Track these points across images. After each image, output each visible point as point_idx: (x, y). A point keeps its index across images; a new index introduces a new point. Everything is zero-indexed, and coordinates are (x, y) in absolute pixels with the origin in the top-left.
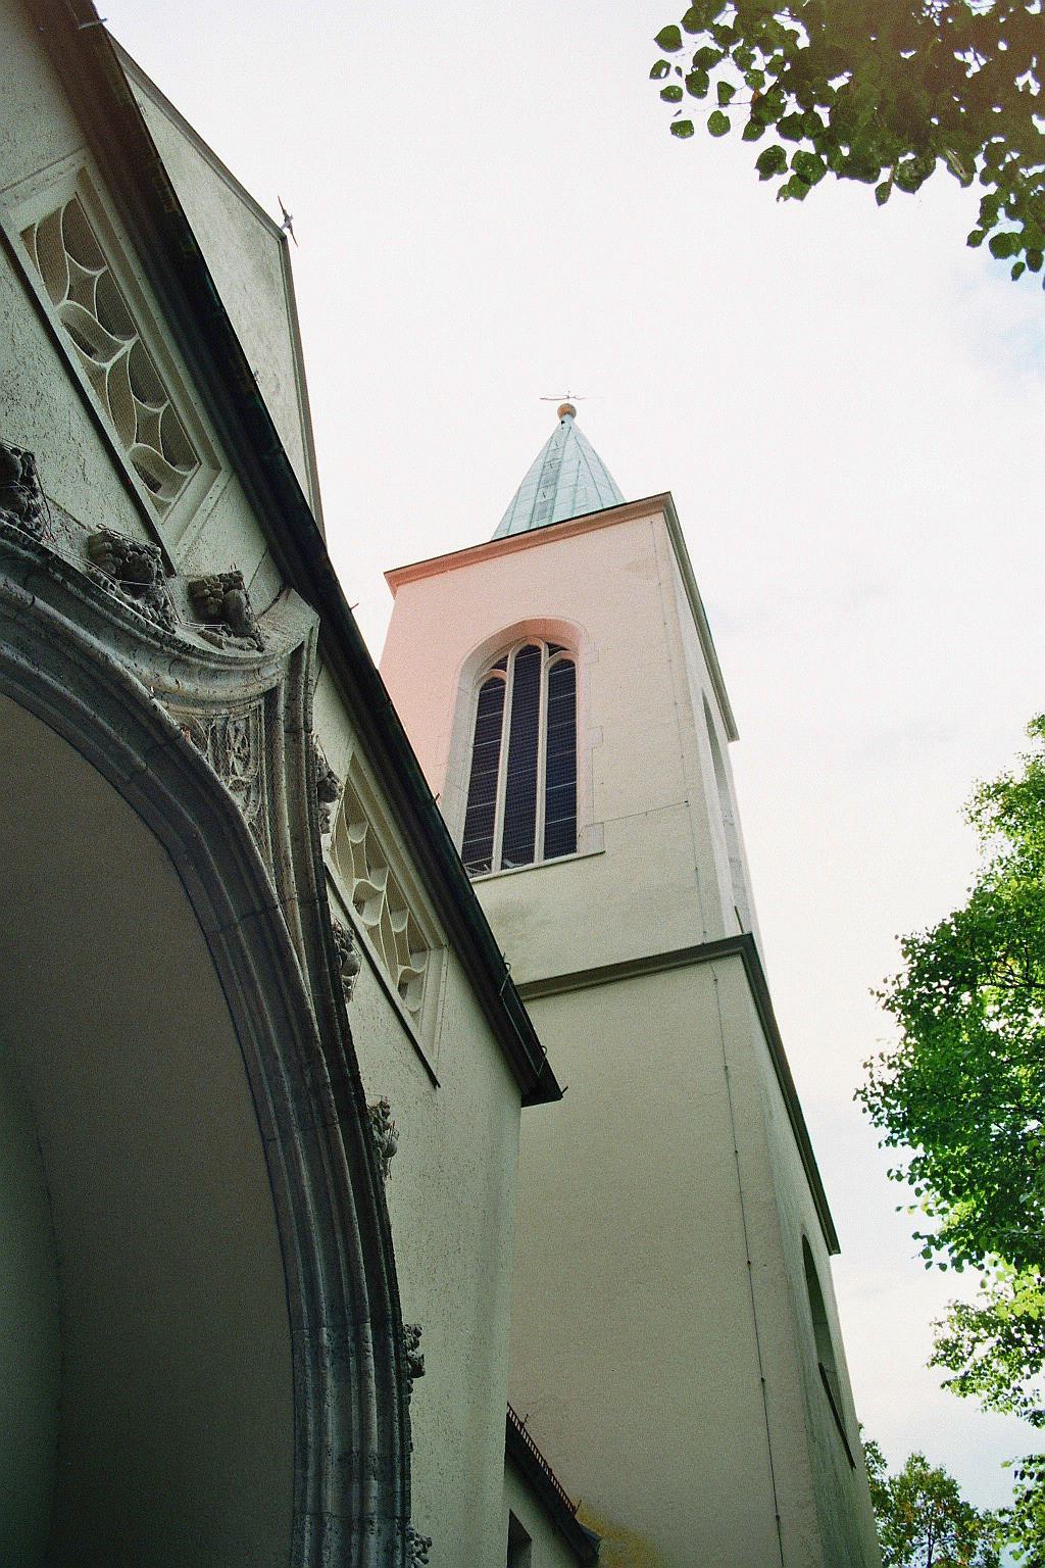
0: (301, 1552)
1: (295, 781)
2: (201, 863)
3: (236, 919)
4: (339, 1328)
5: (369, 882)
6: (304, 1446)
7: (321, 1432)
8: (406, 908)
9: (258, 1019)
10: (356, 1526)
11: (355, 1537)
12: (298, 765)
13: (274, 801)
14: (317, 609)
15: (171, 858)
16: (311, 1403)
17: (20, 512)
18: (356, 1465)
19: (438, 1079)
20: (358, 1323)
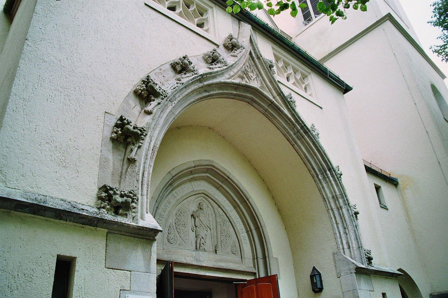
0: (331, 216)
1: (264, 69)
2: (255, 102)
3: (267, 108)
4: (322, 174)
5: (289, 73)
6: (324, 198)
7: (326, 195)
8: (298, 71)
9: (280, 124)
10: (340, 208)
11: (340, 211)
12: (263, 65)
13: (262, 77)
14: (249, 23)
15: (249, 103)
16: (322, 190)
17: (193, 71)
18: (336, 198)
19: (322, 107)
20: (325, 172)
